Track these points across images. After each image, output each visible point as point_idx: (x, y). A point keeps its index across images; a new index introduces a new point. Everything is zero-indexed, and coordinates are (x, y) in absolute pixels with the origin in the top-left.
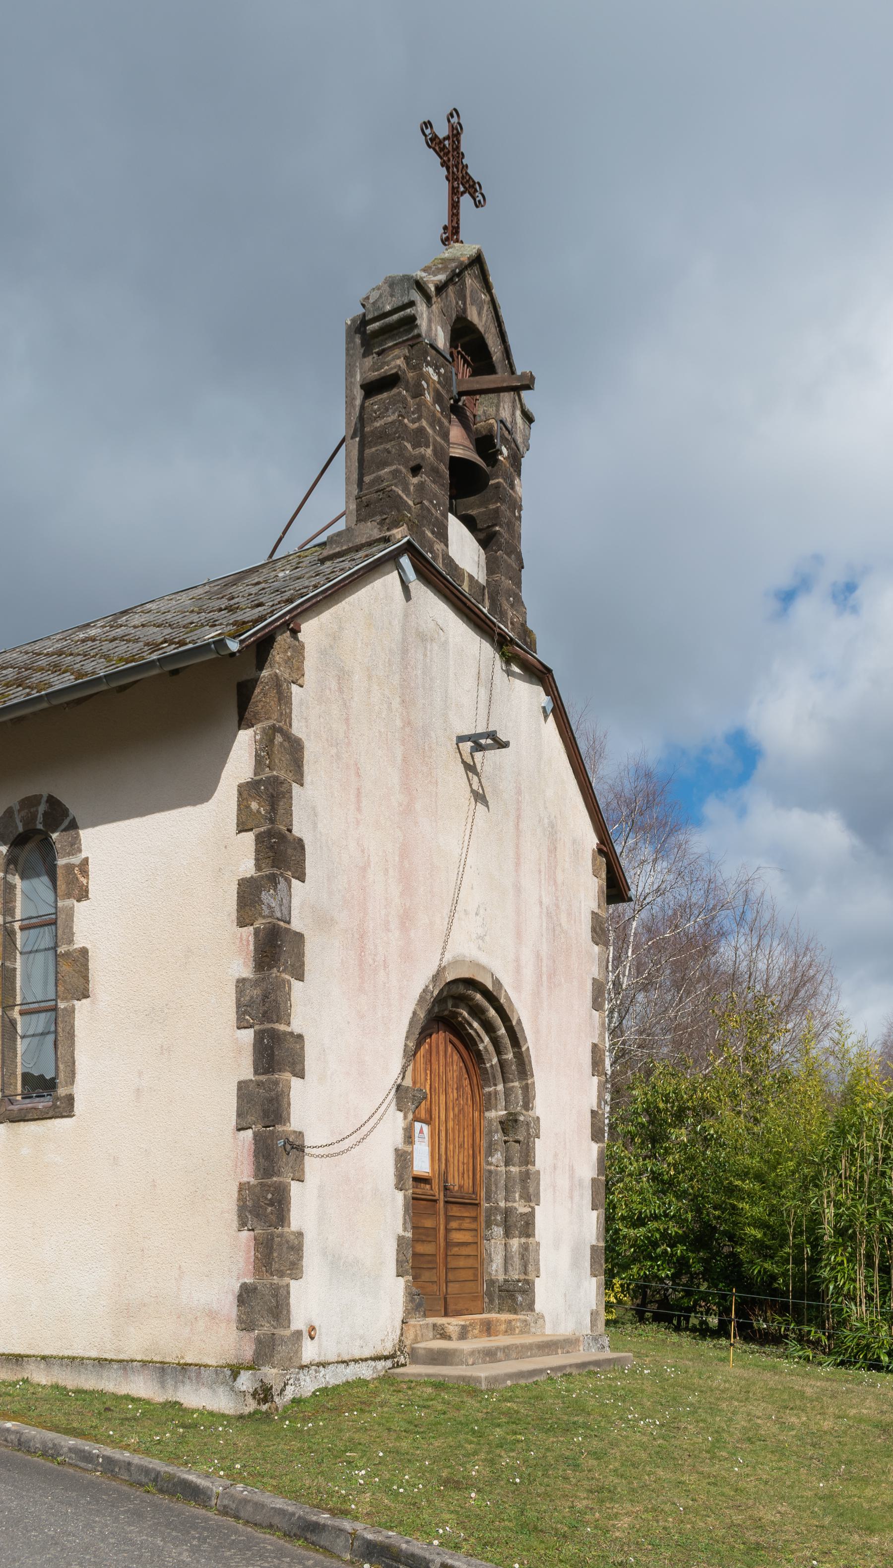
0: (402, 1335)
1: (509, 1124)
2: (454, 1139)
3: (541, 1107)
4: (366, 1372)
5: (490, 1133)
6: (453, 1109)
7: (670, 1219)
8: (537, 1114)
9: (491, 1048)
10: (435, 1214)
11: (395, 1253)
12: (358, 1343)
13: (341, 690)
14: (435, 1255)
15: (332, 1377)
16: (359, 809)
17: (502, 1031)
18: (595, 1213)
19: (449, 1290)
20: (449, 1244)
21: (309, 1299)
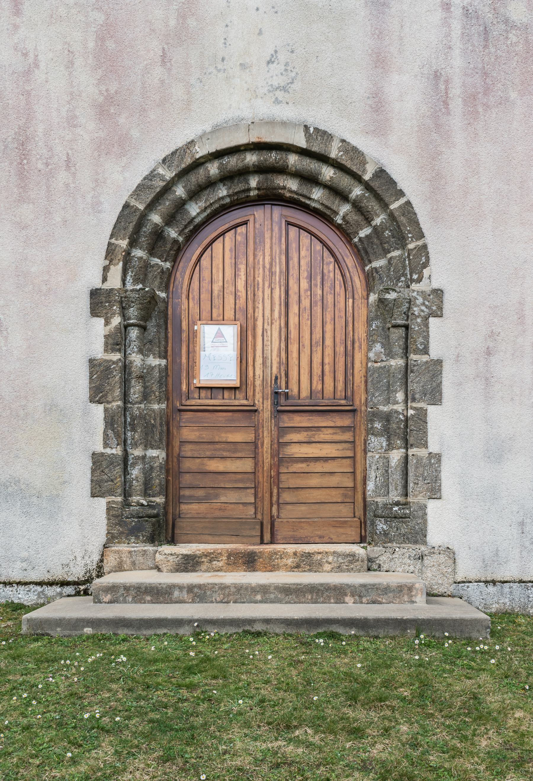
0: (102, 561)
9: (354, 217)
11: (89, 472)
12: (19, 565)
17: (223, 192)
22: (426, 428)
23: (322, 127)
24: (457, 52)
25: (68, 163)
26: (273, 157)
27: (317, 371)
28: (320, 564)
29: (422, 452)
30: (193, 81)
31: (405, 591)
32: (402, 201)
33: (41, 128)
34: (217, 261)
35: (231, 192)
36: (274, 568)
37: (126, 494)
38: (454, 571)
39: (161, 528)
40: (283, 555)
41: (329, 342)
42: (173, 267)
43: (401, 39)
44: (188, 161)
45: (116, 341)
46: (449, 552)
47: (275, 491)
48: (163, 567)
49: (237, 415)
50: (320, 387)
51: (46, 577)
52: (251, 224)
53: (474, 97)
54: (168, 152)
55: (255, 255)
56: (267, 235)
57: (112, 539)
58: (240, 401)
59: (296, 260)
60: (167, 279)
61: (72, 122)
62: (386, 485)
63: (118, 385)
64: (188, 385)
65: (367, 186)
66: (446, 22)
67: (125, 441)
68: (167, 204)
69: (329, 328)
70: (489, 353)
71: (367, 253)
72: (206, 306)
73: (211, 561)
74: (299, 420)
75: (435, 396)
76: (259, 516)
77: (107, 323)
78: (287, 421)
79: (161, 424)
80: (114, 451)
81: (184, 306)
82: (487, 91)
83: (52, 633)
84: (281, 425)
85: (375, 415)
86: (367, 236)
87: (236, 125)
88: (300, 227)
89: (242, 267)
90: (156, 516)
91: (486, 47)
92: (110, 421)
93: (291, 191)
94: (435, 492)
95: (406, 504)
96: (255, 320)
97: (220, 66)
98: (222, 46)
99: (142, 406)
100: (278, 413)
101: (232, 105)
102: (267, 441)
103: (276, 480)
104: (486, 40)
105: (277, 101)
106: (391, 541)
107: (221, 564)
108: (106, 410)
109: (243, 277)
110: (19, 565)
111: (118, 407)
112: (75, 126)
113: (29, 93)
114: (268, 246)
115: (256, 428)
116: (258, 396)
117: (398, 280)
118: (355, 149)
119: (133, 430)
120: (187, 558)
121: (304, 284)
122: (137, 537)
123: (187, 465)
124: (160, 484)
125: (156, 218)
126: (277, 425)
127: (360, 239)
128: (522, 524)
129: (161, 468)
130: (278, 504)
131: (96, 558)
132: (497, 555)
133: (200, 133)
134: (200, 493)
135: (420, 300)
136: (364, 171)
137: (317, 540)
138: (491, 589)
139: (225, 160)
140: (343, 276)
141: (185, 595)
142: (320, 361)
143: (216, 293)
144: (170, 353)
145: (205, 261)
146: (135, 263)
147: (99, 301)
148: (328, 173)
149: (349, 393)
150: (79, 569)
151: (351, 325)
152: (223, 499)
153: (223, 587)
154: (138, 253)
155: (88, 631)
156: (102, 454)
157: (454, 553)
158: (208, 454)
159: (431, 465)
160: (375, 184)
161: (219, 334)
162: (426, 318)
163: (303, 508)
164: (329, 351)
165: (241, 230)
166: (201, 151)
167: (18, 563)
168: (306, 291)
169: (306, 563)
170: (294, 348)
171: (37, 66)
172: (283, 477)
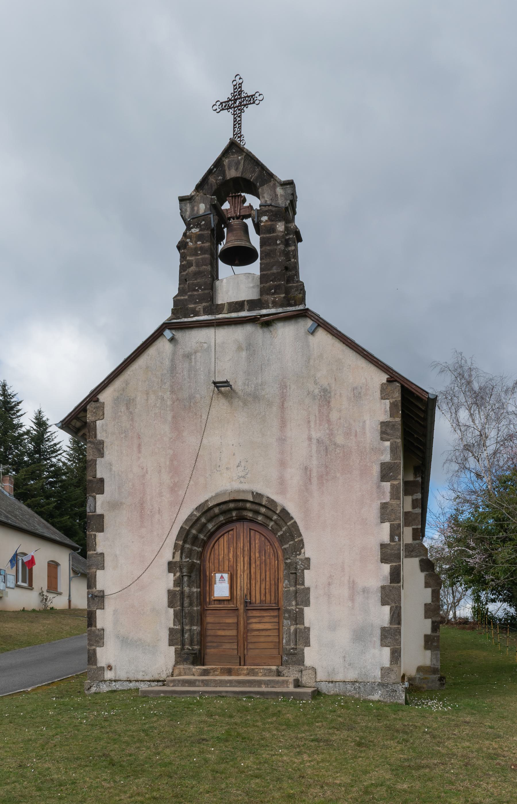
3: (308, 551)
4: (144, 687)
8: (307, 556)
9: (275, 527)
12: (141, 673)
13: (128, 408)
16: (140, 452)
17: (222, 518)
23: (259, 492)
24: (314, 458)
26: (240, 504)
27: (263, 591)
29: (301, 627)
30: (207, 476)
31: (285, 683)
32: (292, 521)
33: (149, 498)
34: (221, 546)
35: (225, 518)
36: (239, 675)
37: (183, 645)
38: (316, 678)
39: (198, 658)
40: (243, 669)
41: (268, 579)
42: (203, 550)
43: (291, 454)
44: (206, 508)
45: (178, 582)
48: (195, 674)
49: (229, 611)
50: (264, 599)
51: (152, 678)
52: (235, 530)
54: (198, 505)
55: (236, 543)
56: (242, 535)
58: (231, 606)
59: (254, 544)
60: (201, 556)
61: (160, 495)
62: (289, 640)
63: (179, 600)
64: (210, 599)
65: (278, 515)
66: (310, 446)
67: (183, 623)
68: (198, 525)
69: (268, 573)
70: (329, 584)
72: (217, 565)
73: (214, 672)
75: (307, 603)
76: (239, 654)
77: (174, 576)
78: (250, 614)
79: (197, 616)
80: (177, 627)
81: (207, 566)
82: (327, 473)
83: (149, 696)
84: (248, 615)
86: (281, 535)
87: (224, 493)
89: (232, 549)
90: (195, 654)
91: (326, 455)
92: (176, 615)
95: (296, 649)
96: (237, 571)
97: (218, 469)
98: (219, 461)
99: (189, 608)
100: (246, 610)
101: (224, 482)
103: (245, 639)
104: (327, 452)
105: (241, 482)
107: (218, 673)
108: (174, 611)
109: (232, 553)
110: (141, 673)
111: (179, 609)
112: (162, 496)
113: (144, 484)
114: (242, 539)
115: (238, 617)
116: (238, 603)
118: (273, 501)
119: (186, 618)
120: (204, 670)
121: (257, 555)
122: (187, 663)
123: (209, 633)
124: (197, 641)
125: (194, 531)
126: (246, 615)
128: (344, 657)
129: (197, 634)
130: (247, 649)
131: (171, 671)
133: (210, 497)
134: (215, 644)
135: (300, 563)
136: (277, 509)
137: (263, 664)
138: (331, 685)
139: (221, 506)
140: (274, 551)
142: (264, 587)
144: (202, 585)
145: (216, 547)
146: (186, 550)
147: (171, 567)
148: (263, 510)
149: (276, 601)
150: (164, 675)
151: (277, 572)
152: (224, 647)
153: (215, 681)
154: (187, 546)
155: (162, 695)
156: (173, 629)
157: (316, 670)
158: (218, 628)
160: (281, 515)
161: (222, 577)
163: (257, 651)
164: (268, 583)
165: (231, 532)
166: (211, 504)
168: (258, 558)
170: (253, 582)
171: (147, 473)
172: (249, 638)
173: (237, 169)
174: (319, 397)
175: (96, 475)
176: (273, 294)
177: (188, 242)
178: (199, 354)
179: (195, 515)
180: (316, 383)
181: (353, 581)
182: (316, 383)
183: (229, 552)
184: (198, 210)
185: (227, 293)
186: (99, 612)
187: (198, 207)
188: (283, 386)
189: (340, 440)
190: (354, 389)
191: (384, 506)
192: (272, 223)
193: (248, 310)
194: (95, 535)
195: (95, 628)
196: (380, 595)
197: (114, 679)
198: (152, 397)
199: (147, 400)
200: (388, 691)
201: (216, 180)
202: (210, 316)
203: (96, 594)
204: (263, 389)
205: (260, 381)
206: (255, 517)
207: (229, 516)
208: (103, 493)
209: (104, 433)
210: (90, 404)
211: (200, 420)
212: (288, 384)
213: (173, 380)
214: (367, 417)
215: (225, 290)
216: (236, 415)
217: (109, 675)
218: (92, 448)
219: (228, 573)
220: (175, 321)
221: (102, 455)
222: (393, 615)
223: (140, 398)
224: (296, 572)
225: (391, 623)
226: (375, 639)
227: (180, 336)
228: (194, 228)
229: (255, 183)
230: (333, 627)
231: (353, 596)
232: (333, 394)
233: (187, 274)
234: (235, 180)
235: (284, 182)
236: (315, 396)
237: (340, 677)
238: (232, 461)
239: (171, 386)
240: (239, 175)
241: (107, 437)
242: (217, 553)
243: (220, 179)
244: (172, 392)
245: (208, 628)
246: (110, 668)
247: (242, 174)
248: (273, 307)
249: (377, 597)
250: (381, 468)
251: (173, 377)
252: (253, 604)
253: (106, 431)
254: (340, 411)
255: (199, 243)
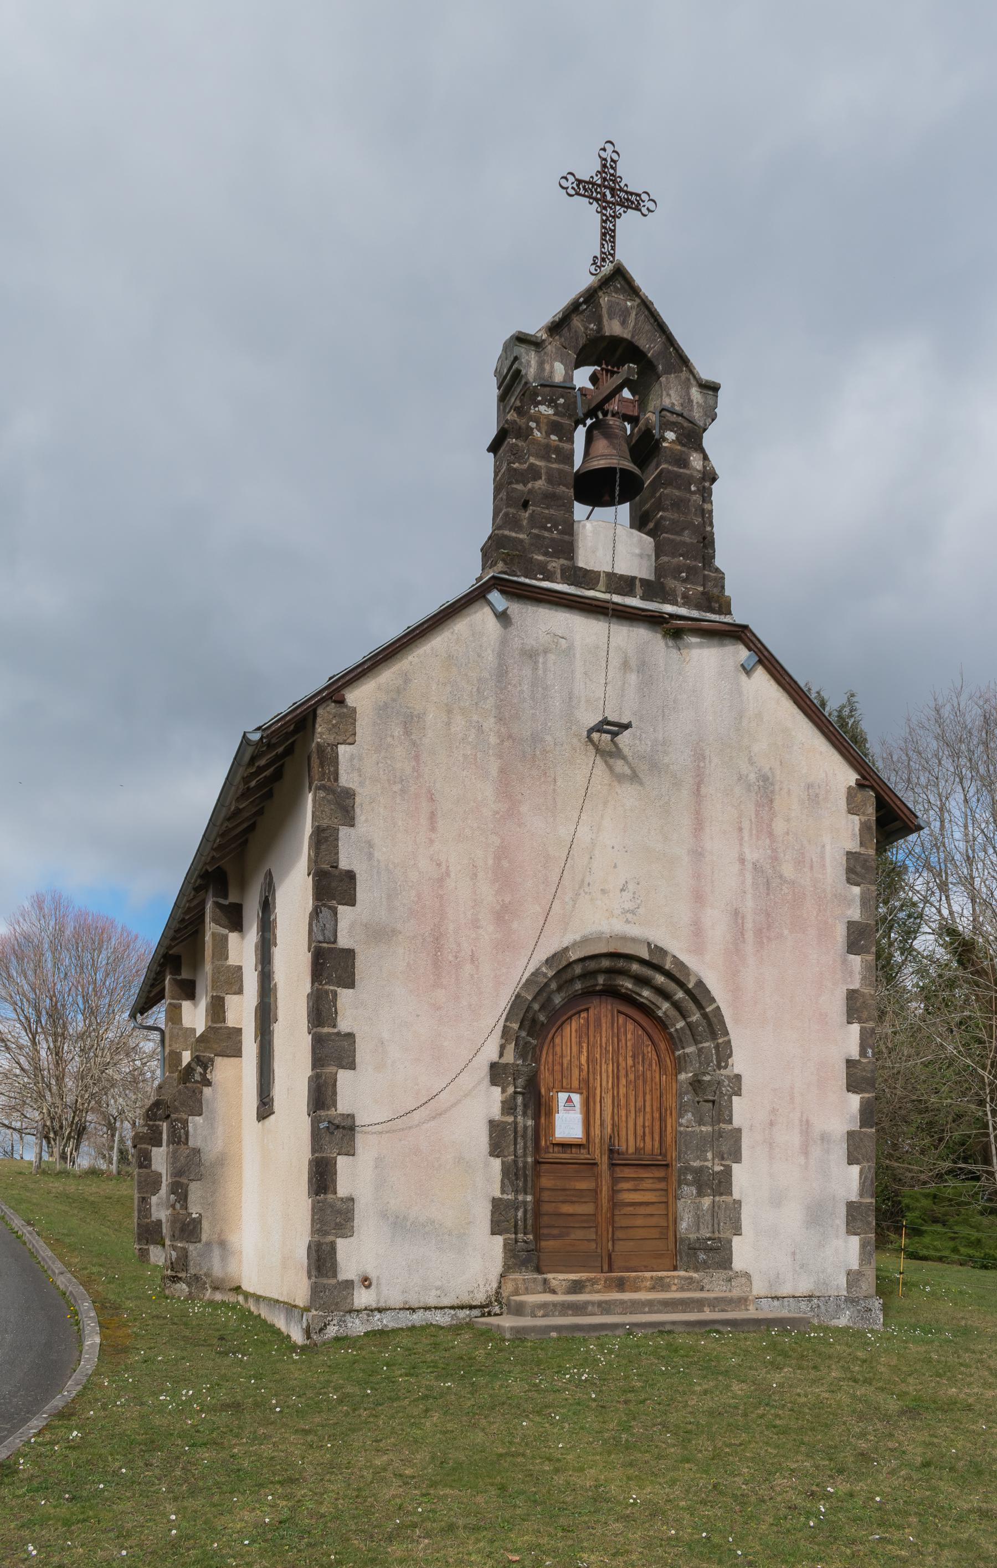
0: (500, 1287)
1: (696, 1084)
2: (627, 1104)
3: (739, 1063)
4: (442, 1319)
5: (680, 1095)
6: (627, 1075)
7: (537, 1175)
8: (736, 1071)
9: (673, 1013)
10: (597, 1177)
11: (489, 1214)
12: (434, 1293)
13: (407, 733)
14: (594, 1215)
15: (378, 1322)
16: (433, 829)
18: (855, 1169)
19: (617, 1248)
20: (615, 1205)
21: (352, 1257)
22: (731, 1180)
24: (749, 896)
25: (473, 958)
26: (621, 964)
27: (640, 1132)
28: (669, 1286)
30: (567, 900)
33: (451, 927)
36: (637, 1289)
40: (644, 1279)
41: (648, 1109)
44: (564, 963)
45: (508, 1107)
46: (747, 1275)
47: (610, 1230)
51: (455, 1302)
52: (591, 1011)
53: (760, 930)
57: (508, 1269)
58: (583, 1155)
59: (623, 1041)
61: (475, 924)
66: (742, 872)
69: (648, 1097)
70: (772, 1124)
71: (681, 1041)
74: (628, 1172)
77: (503, 1091)
78: (620, 1172)
80: (509, 1197)
82: (769, 927)
85: (687, 1169)
87: (598, 938)
88: (627, 1015)
89: (585, 1045)
91: (768, 894)
92: (505, 1172)
93: (627, 989)
94: (738, 1232)
100: (612, 1165)
101: (599, 918)
102: (604, 1188)
103: (612, 1221)
105: (627, 922)
106: (709, 1268)
107: (600, 1287)
108: (503, 1163)
109: (585, 1054)
112: (478, 927)
117: (708, 1065)
118: (682, 964)
121: (630, 1062)
122: (527, 1267)
125: (536, 1006)
127: (676, 1030)
128: (794, 1254)
131: (495, 1285)
132: (778, 1277)
133: (572, 941)
134: (555, 1232)
135: (726, 1083)
136: (689, 981)
138: (776, 1303)
139: (587, 963)
141: (596, 1309)
143: (565, 1065)
145: (557, 1040)
147: (497, 1073)
152: (573, 1236)
153: (622, 1302)
155: (554, 1334)
156: (500, 1199)
158: (561, 1199)
159: (735, 1209)
161: (569, 1100)
162: (730, 1097)
163: (632, 1243)
165: (584, 1015)
166: (573, 956)
167: (434, 1291)
169: (659, 1284)
171: (448, 875)
172: (617, 1218)
173: (624, 323)
174: (756, 787)
175: (337, 861)
176: (685, 581)
177: (532, 429)
178: (552, 657)
179: (545, 975)
180: (751, 762)
181: (807, 1121)
182: (751, 762)
183: (580, 1052)
184: (552, 372)
185: (594, 552)
186: (342, 1161)
187: (552, 367)
188: (699, 756)
189: (788, 870)
190: (809, 786)
191: (852, 995)
192: (683, 449)
193: (642, 598)
194: (335, 994)
195: (334, 1197)
196: (846, 1146)
197: (374, 1306)
198: (459, 723)
199: (448, 724)
200: (859, 1311)
201: (586, 328)
202: (572, 587)
203: (336, 1122)
204: (666, 753)
205: (660, 738)
206: (637, 989)
207: (591, 982)
208: (354, 905)
209: (356, 774)
210: (324, 705)
211: (552, 787)
212: (707, 753)
213: (502, 697)
214: (827, 839)
215: (590, 544)
216: (619, 792)
217: (363, 1298)
218: (328, 801)
219: (581, 1093)
220: (507, 577)
221: (350, 821)
222: (864, 1182)
223: (433, 717)
224: (714, 1096)
225: (861, 1195)
226: (838, 1222)
227: (516, 611)
228: (544, 404)
229: (656, 363)
230: (777, 1200)
231: (807, 1146)
232: (777, 788)
233: (530, 491)
234: (616, 341)
235: (707, 381)
236: (750, 785)
237: (786, 1290)
238: (619, 882)
239: (498, 707)
240: (626, 335)
241: (362, 784)
242: (559, 1053)
243: (592, 329)
244: (500, 719)
245: (543, 1198)
246: (366, 1282)
247: (633, 336)
248: (684, 605)
249: (840, 1151)
250: (848, 930)
251: (501, 689)
252: (623, 1154)
253: (359, 770)
254: (788, 820)
255: (553, 437)
